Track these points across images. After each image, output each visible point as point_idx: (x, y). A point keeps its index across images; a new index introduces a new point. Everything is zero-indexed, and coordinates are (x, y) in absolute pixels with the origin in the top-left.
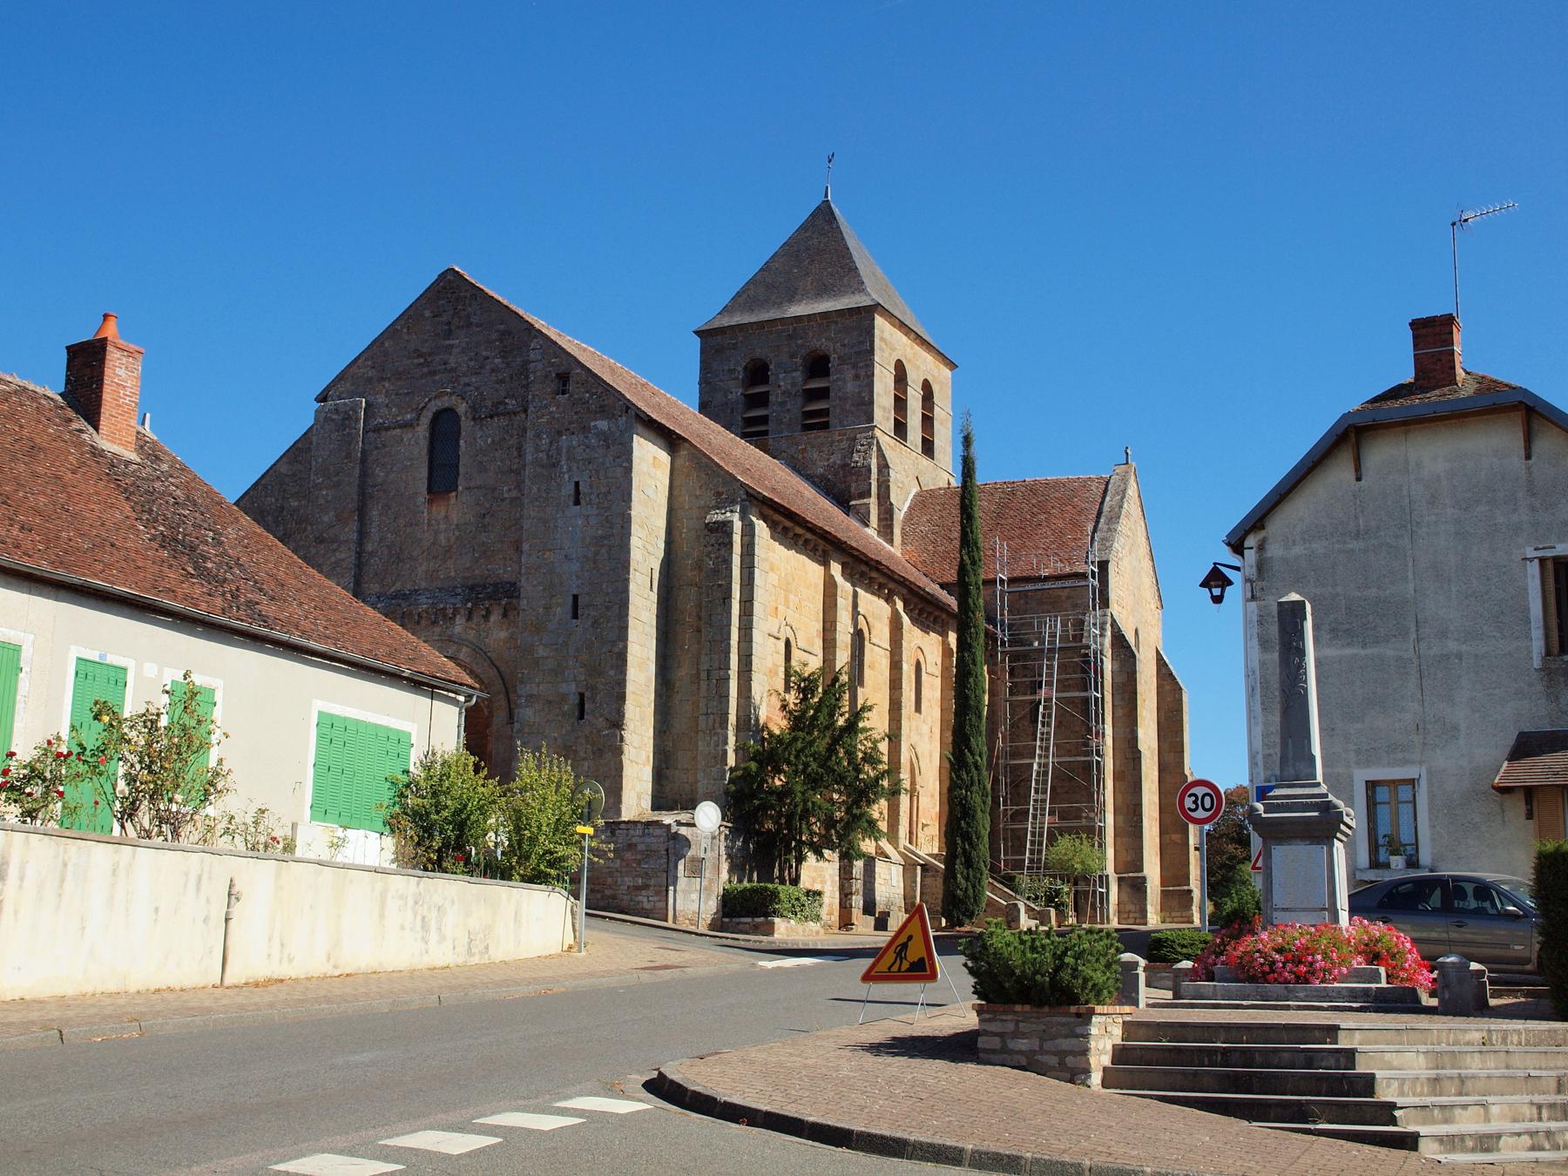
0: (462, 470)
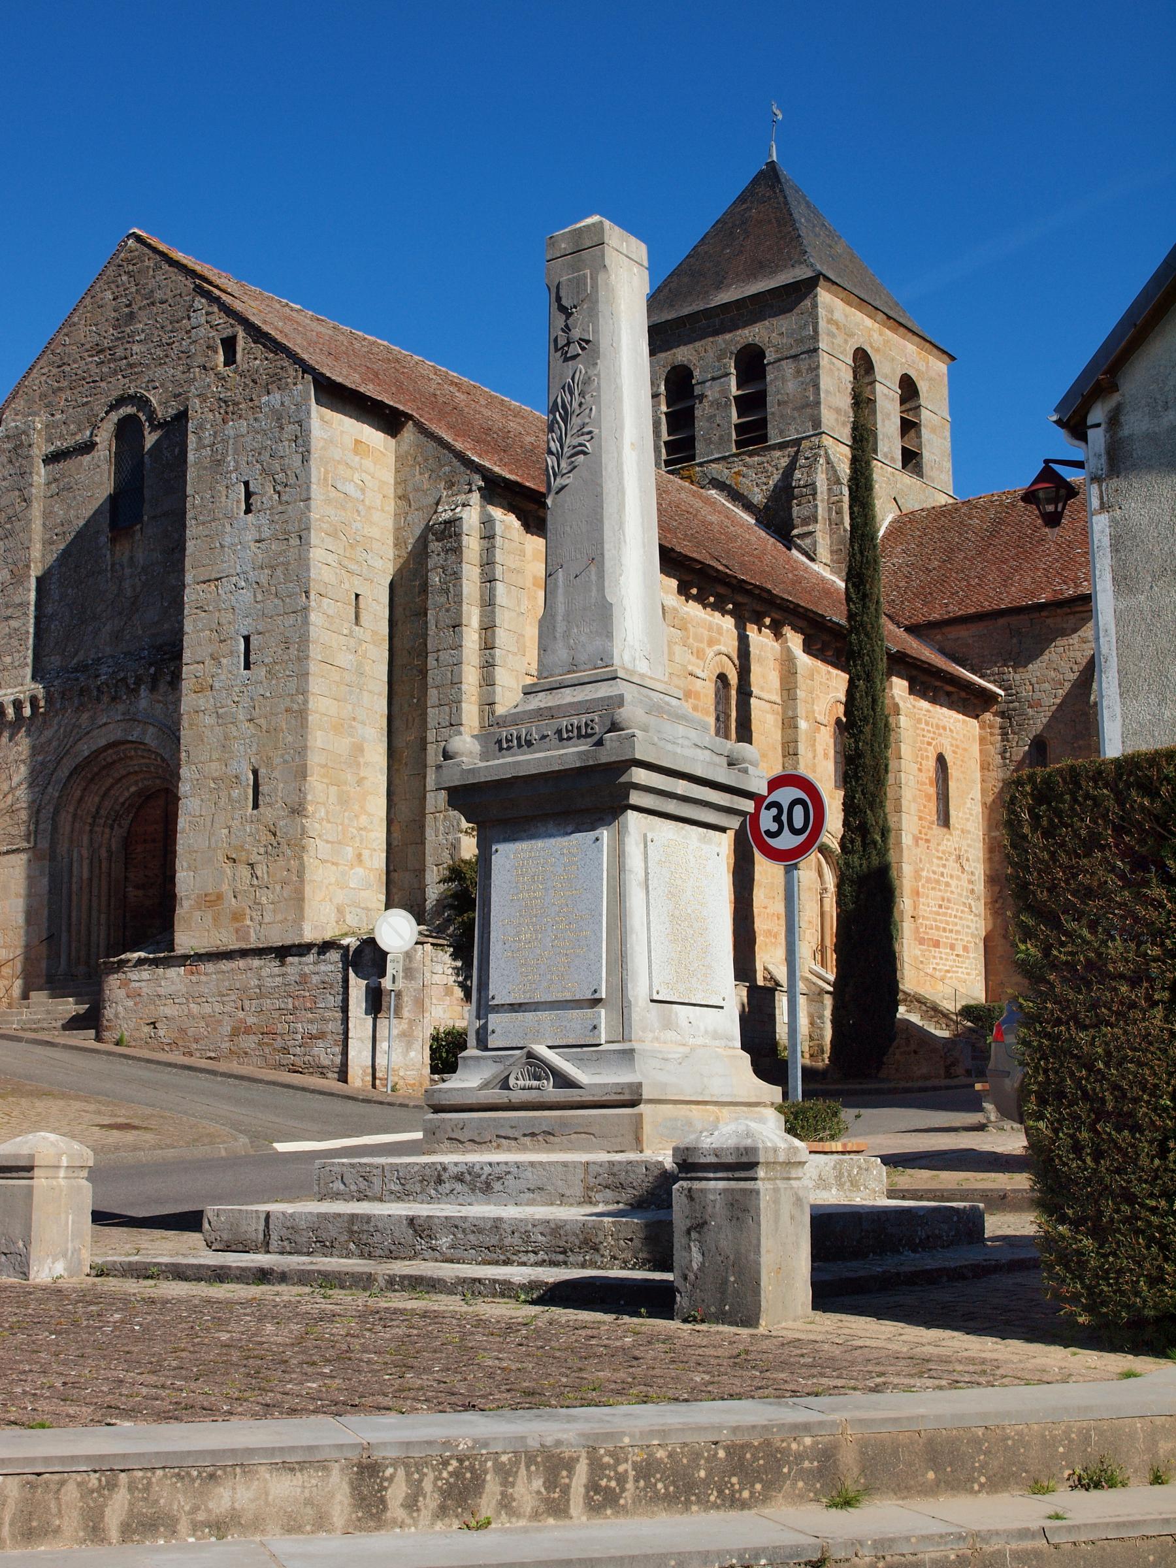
0: (147, 493)
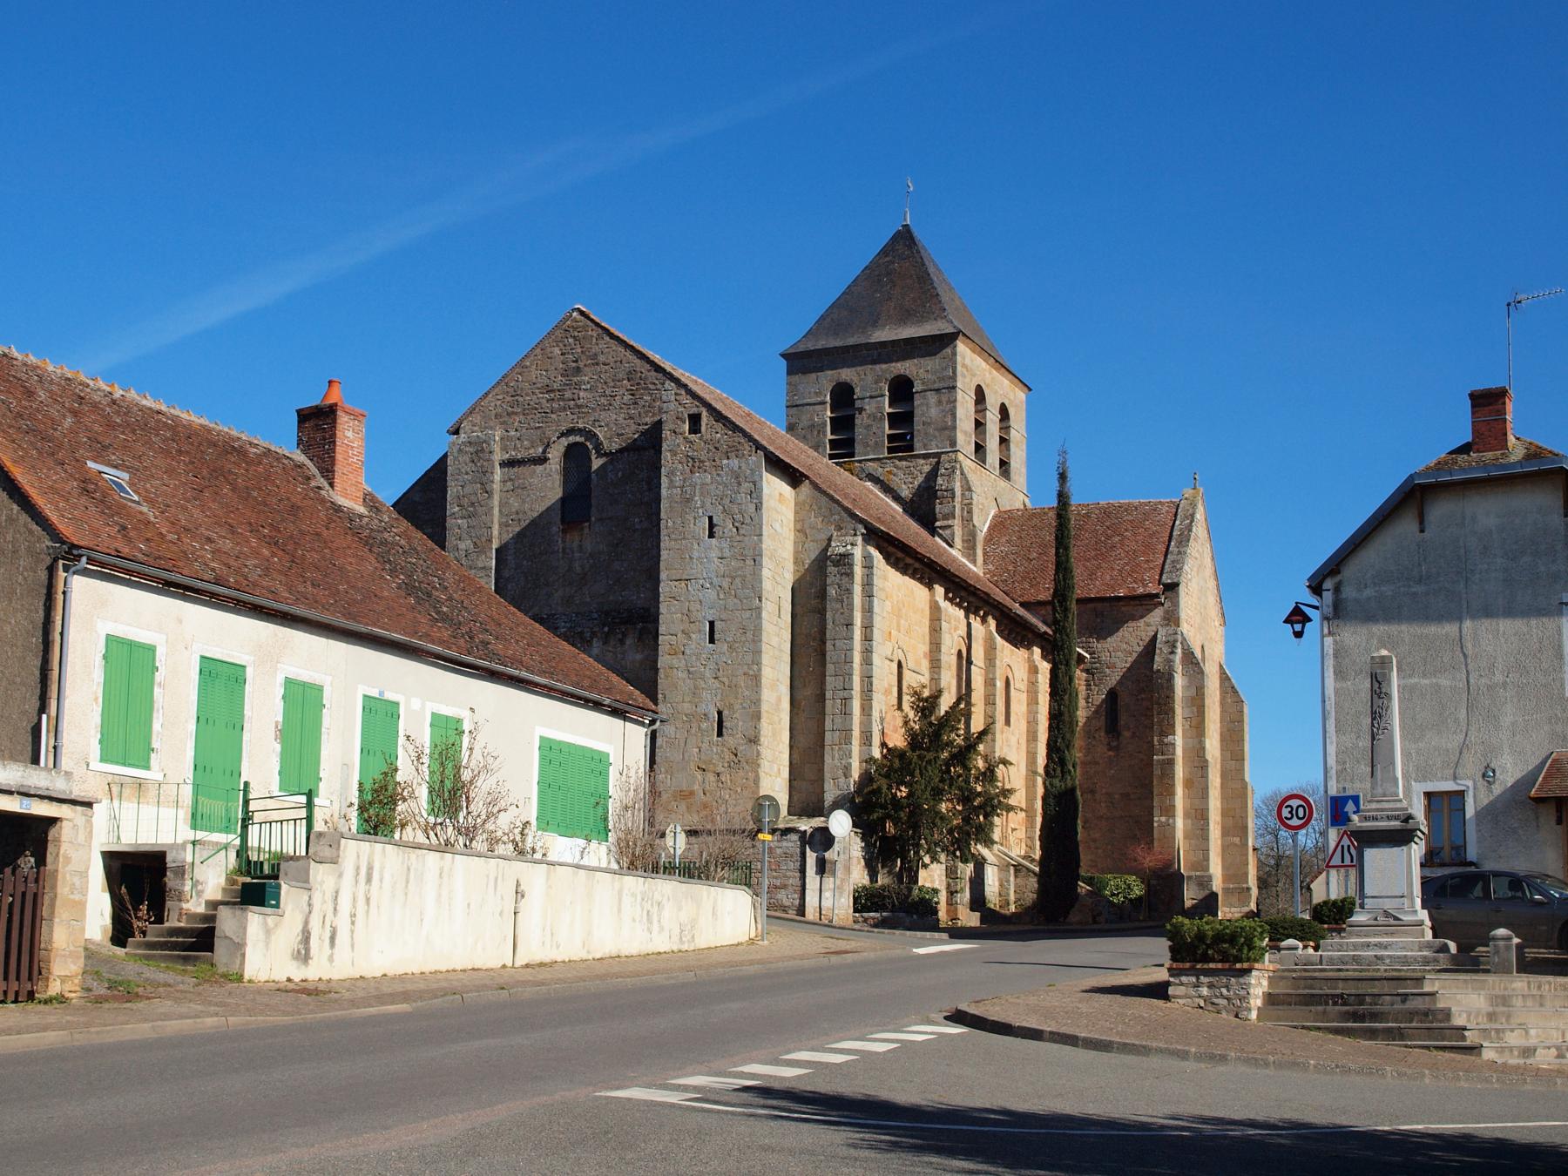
0: (594, 502)
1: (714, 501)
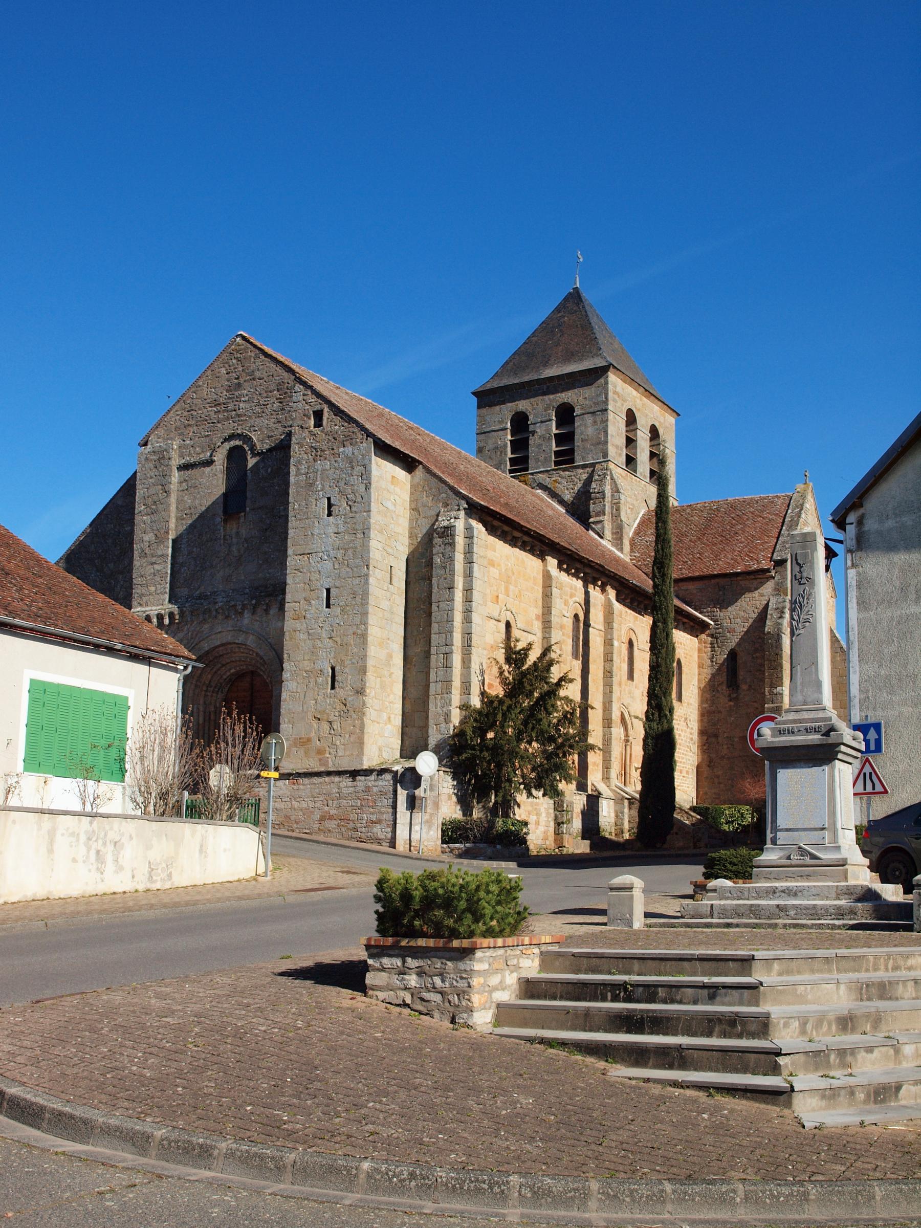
0: (249, 494)
1: (332, 484)
